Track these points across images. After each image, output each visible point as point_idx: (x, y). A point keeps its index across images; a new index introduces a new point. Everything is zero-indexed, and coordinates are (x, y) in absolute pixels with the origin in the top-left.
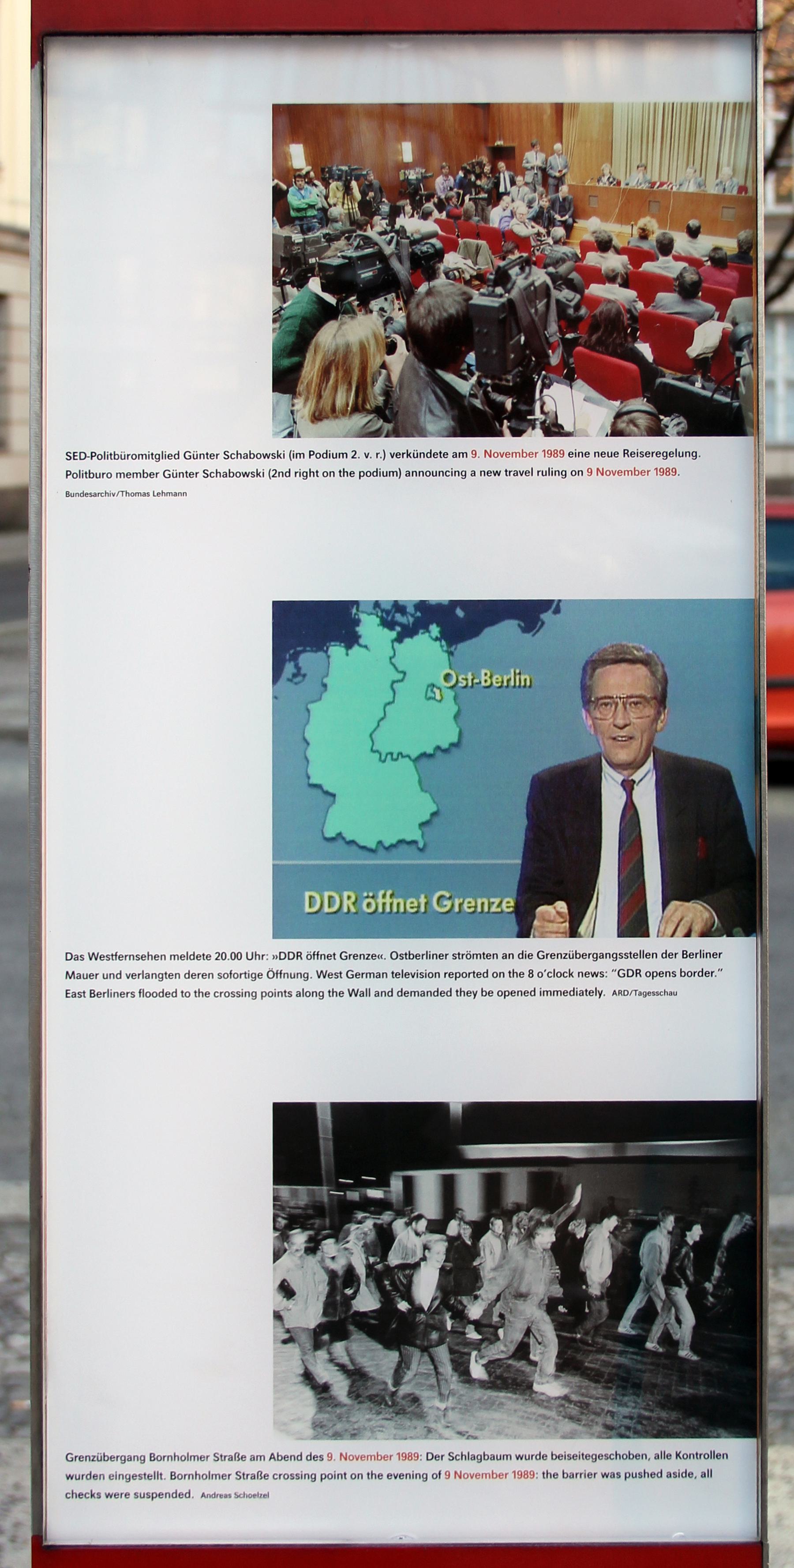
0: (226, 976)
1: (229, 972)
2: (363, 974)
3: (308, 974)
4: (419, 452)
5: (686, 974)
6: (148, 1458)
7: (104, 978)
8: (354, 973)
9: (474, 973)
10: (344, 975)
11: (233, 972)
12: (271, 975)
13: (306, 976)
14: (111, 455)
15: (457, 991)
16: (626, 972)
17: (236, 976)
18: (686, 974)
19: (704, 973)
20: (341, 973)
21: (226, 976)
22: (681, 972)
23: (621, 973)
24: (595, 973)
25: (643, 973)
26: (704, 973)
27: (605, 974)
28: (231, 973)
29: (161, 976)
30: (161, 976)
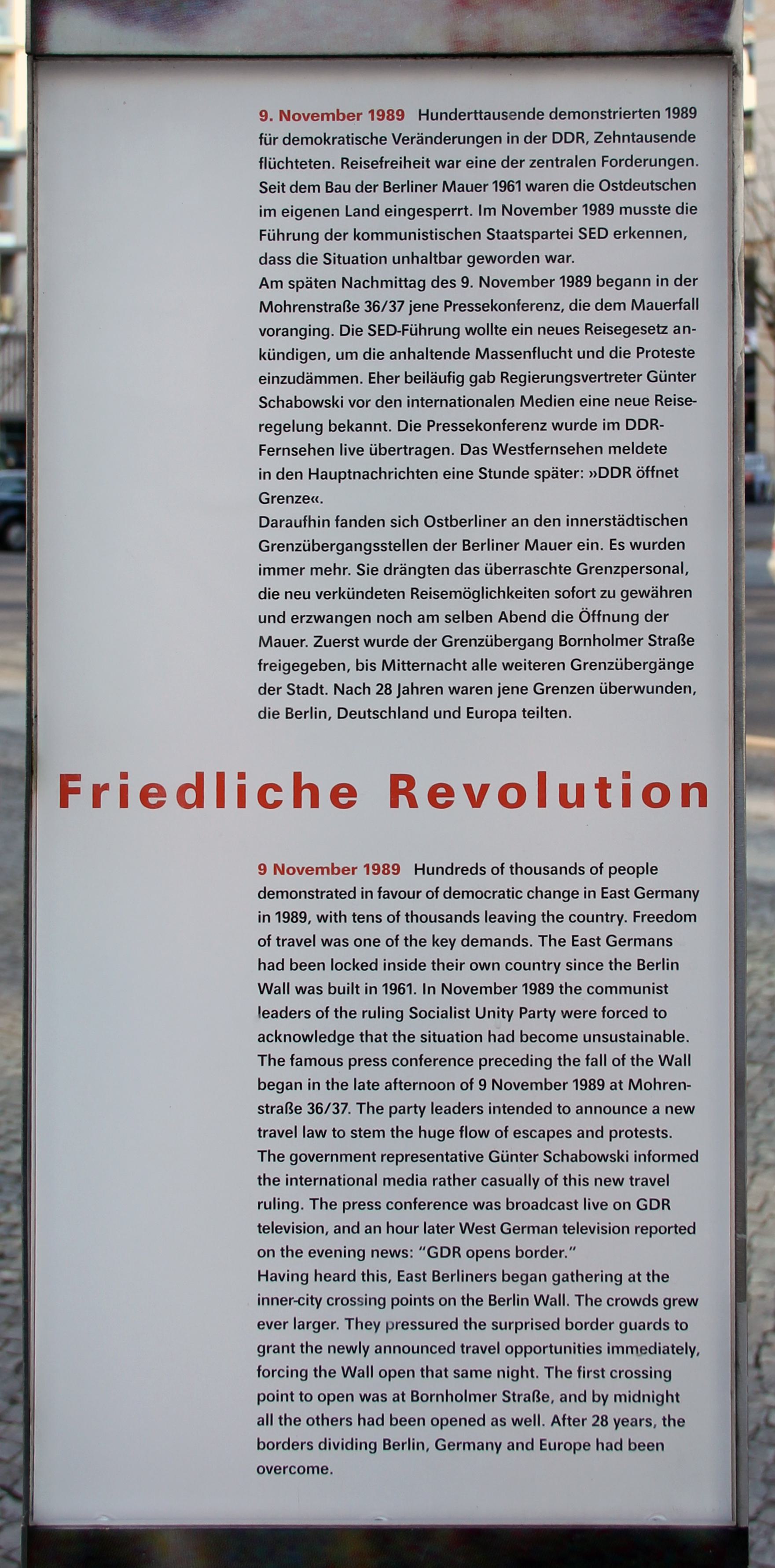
0: (566, 594)
1: (570, 590)
2: (657, 892)
3: (297, 1203)
4: (272, 136)
5: (266, 1446)
6: (380, 1446)
7: (479, 233)
8: (617, 940)
9: (558, 232)
10: (603, 942)
11: (652, 1153)
12: (585, 617)
13: (295, 1205)
14: (335, 915)
15: (363, 1274)
16: (648, 1203)
17: (266, 1373)
18: (266, 1446)
19: (675, 689)
20: (598, 939)
21: (566, 594)
22: (330, 988)
23: (432, 1251)
24: (319, 616)
25: (463, 1252)
26: (675, 689)
27: (409, 1253)
28: (649, 1155)
29: (422, 571)
30: (422, 571)
